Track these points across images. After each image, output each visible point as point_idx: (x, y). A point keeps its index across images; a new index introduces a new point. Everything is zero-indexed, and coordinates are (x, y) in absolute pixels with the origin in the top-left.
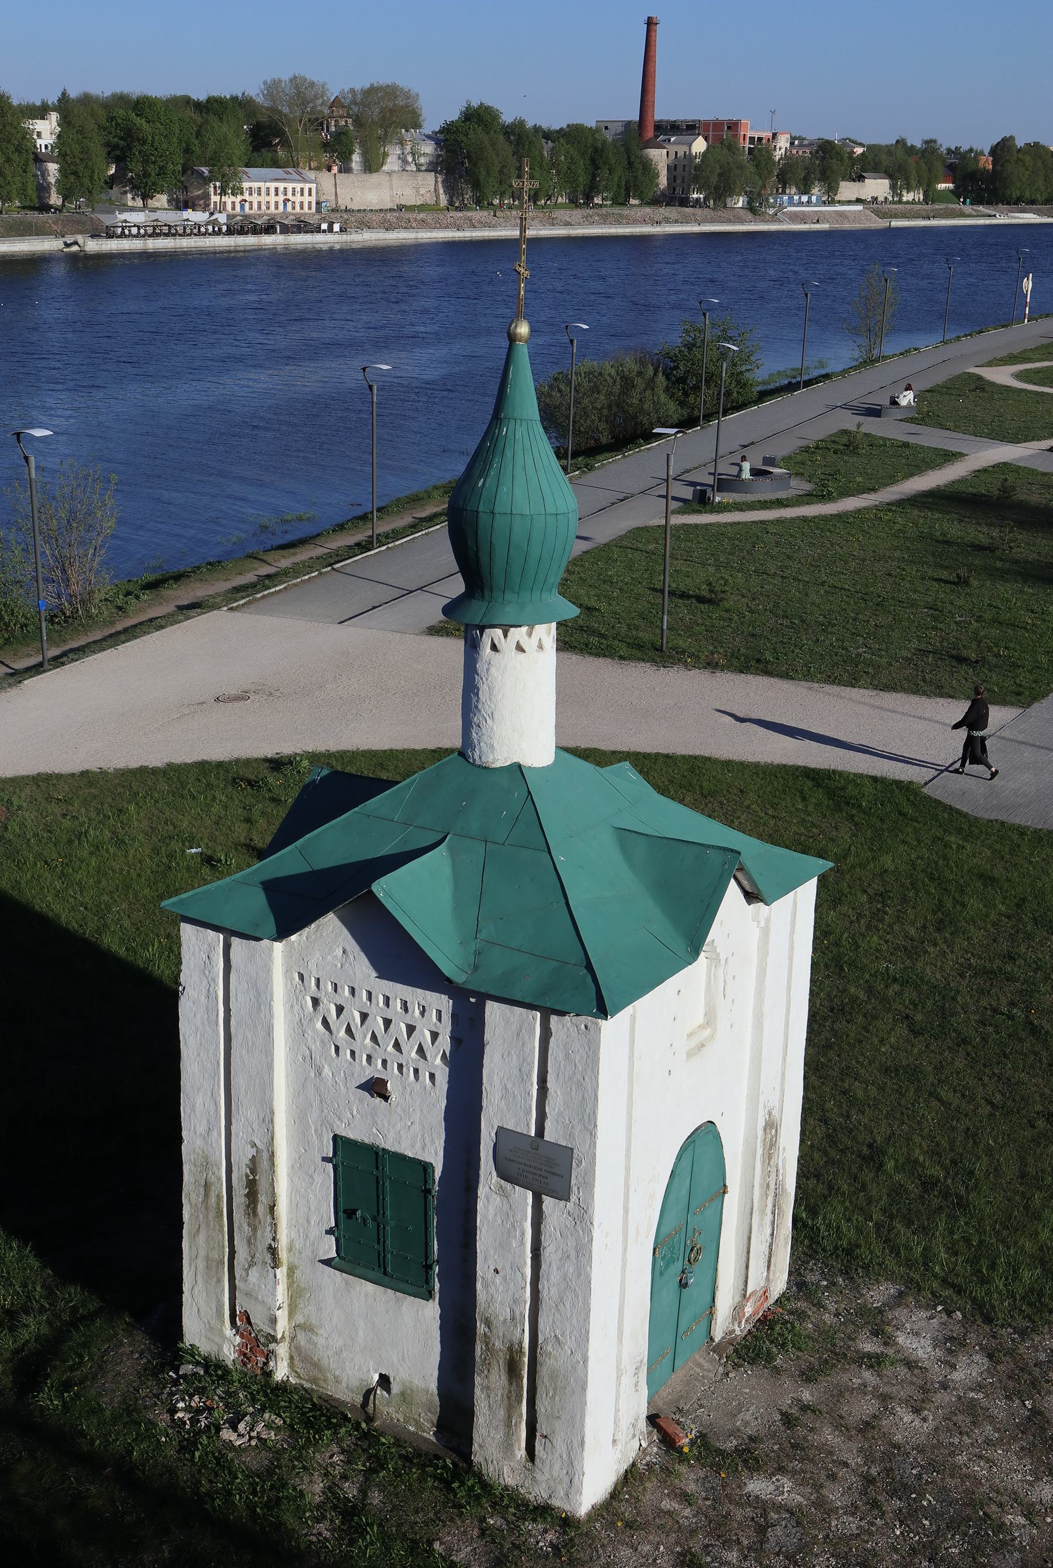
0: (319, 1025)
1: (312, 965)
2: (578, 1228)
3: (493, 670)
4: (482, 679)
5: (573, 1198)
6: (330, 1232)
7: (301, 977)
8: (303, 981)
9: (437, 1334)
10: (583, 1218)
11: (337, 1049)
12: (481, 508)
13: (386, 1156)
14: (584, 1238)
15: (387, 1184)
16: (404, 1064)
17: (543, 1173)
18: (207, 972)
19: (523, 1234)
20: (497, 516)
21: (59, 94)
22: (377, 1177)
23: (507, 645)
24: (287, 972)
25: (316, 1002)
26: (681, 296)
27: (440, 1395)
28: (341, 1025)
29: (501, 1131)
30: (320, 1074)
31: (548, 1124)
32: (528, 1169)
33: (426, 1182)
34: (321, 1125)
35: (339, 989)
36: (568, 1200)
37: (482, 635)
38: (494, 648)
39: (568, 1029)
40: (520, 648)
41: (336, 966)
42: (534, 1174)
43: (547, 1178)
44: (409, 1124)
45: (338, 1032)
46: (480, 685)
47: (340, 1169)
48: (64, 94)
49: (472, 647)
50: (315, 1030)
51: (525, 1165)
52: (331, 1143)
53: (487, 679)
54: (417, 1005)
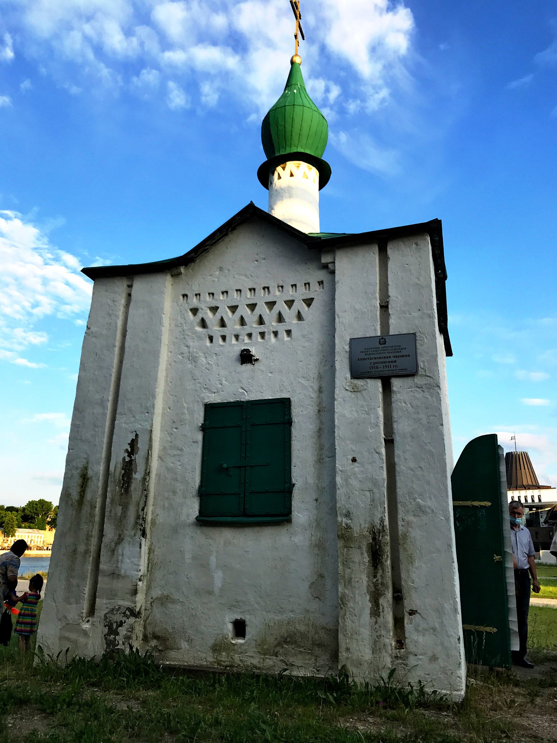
17: (393, 359)
31: (393, 321)
38: (279, 177)
42: (384, 362)
43: (395, 362)
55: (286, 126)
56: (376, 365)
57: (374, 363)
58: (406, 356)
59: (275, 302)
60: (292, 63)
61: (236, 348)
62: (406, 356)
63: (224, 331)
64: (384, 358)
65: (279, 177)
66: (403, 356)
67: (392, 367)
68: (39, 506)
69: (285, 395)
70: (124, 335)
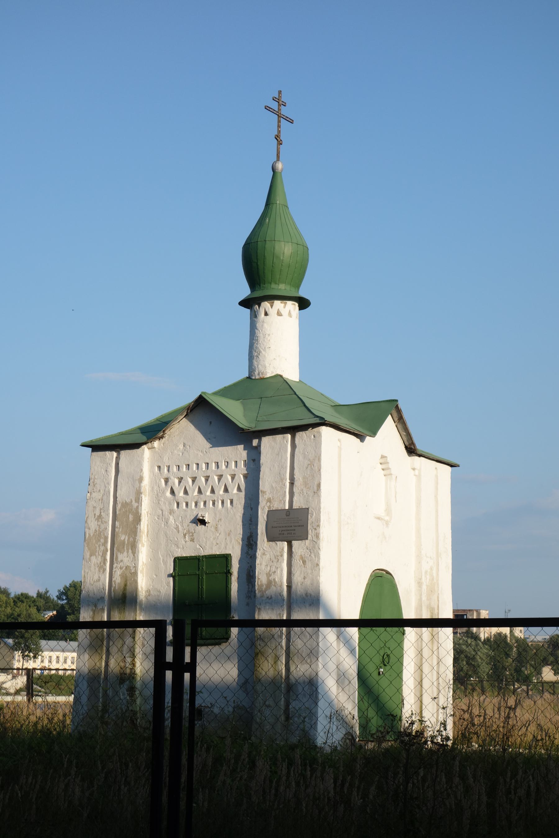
0: (168, 494)
1: (166, 459)
2: (313, 555)
3: (265, 325)
4: (259, 331)
5: (310, 537)
6: (170, 575)
7: (159, 467)
8: (160, 471)
9: (241, 523)
10: (315, 550)
11: (178, 504)
12: (259, 240)
13: (204, 559)
14: (316, 559)
15: (204, 577)
16: (216, 500)
17: (293, 528)
18: (104, 480)
19: (282, 570)
20: (267, 242)
21: (37, 592)
22: (199, 575)
23: (272, 312)
24: (152, 467)
25: (167, 481)
26: (309, 779)
27: (238, 600)
28: (181, 489)
29: (271, 513)
30: (167, 523)
31: (295, 499)
32: (284, 529)
33: (227, 566)
34: (167, 556)
35: (180, 468)
36: (307, 539)
37: (259, 308)
38: (266, 314)
39: (305, 441)
40: (279, 314)
41: (179, 455)
42: (288, 530)
43: (295, 530)
44: (218, 535)
45: (179, 493)
46: (259, 335)
47: (177, 578)
48: (38, 591)
49: (254, 315)
50: (166, 498)
51: (283, 527)
52: (172, 564)
53: (262, 331)
54: (224, 463)
55: (259, 263)
56: (283, 532)
57: (282, 531)
58: (301, 526)
59: (223, 475)
60: (274, 169)
61: (193, 512)
62: (301, 526)
63: (214, 497)
64: (286, 527)
65: (266, 314)
66: (299, 526)
67: (292, 533)
68: (9, 714)
69: (227, 552)
70: (292, 484)
